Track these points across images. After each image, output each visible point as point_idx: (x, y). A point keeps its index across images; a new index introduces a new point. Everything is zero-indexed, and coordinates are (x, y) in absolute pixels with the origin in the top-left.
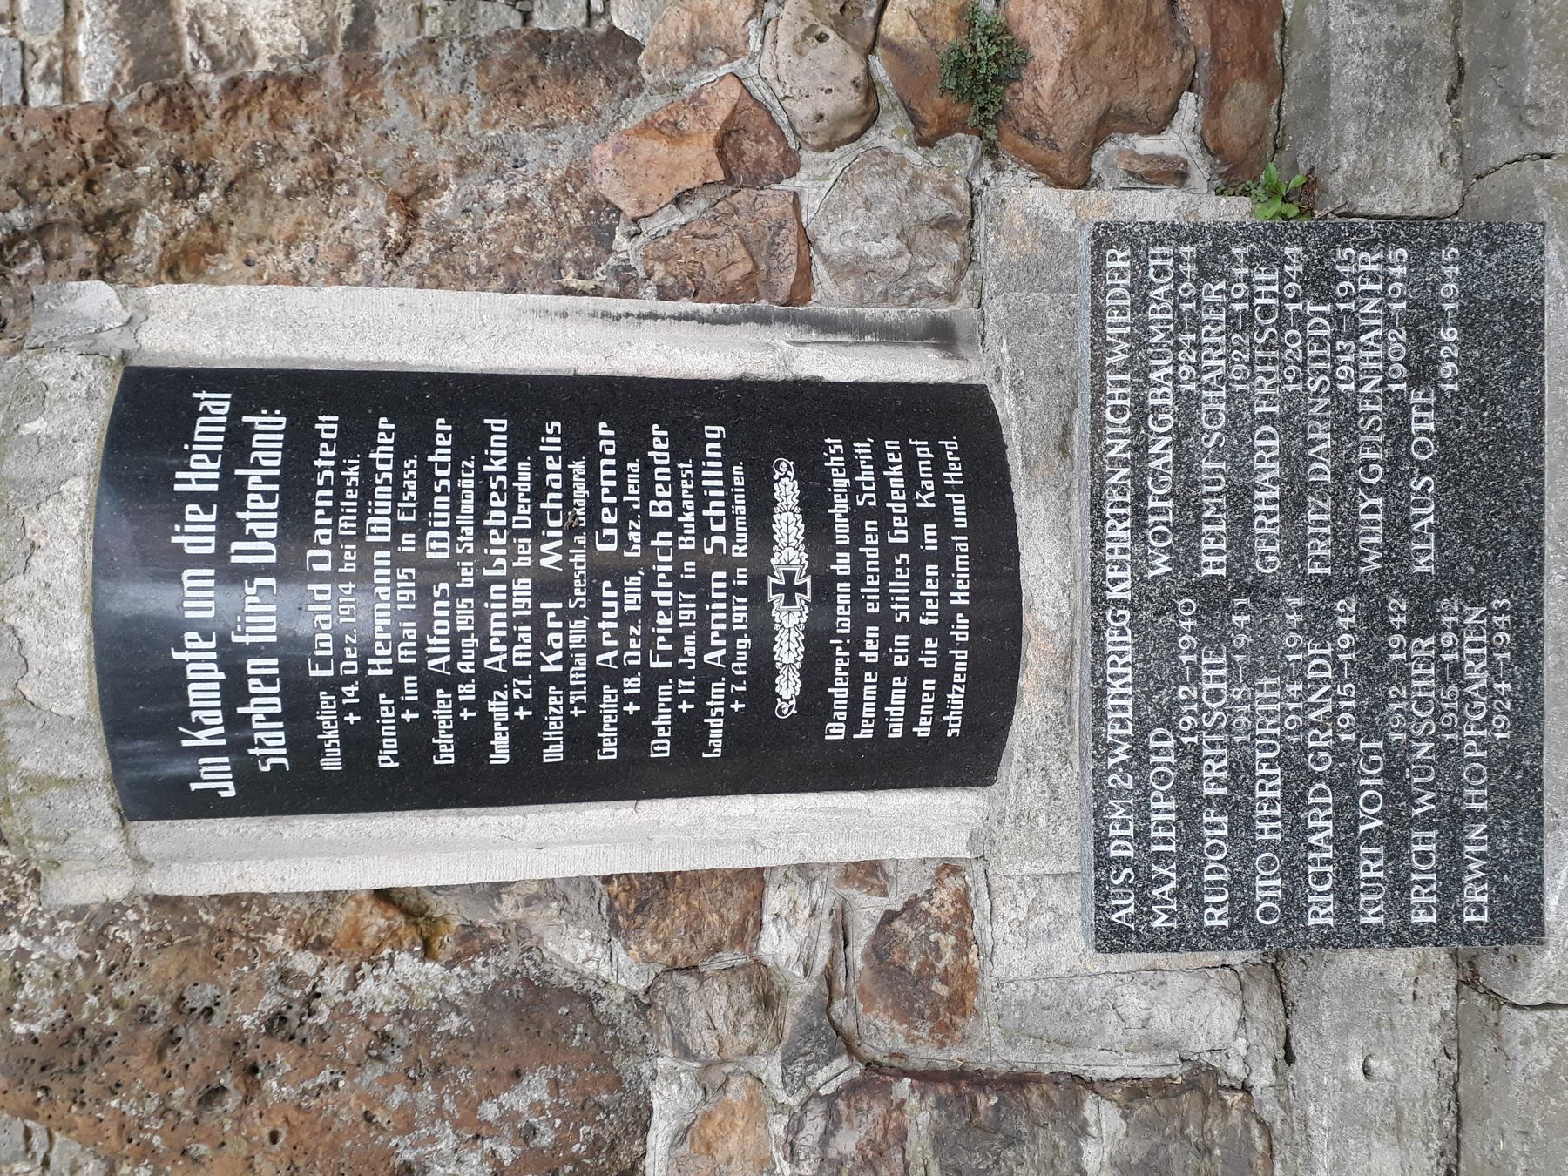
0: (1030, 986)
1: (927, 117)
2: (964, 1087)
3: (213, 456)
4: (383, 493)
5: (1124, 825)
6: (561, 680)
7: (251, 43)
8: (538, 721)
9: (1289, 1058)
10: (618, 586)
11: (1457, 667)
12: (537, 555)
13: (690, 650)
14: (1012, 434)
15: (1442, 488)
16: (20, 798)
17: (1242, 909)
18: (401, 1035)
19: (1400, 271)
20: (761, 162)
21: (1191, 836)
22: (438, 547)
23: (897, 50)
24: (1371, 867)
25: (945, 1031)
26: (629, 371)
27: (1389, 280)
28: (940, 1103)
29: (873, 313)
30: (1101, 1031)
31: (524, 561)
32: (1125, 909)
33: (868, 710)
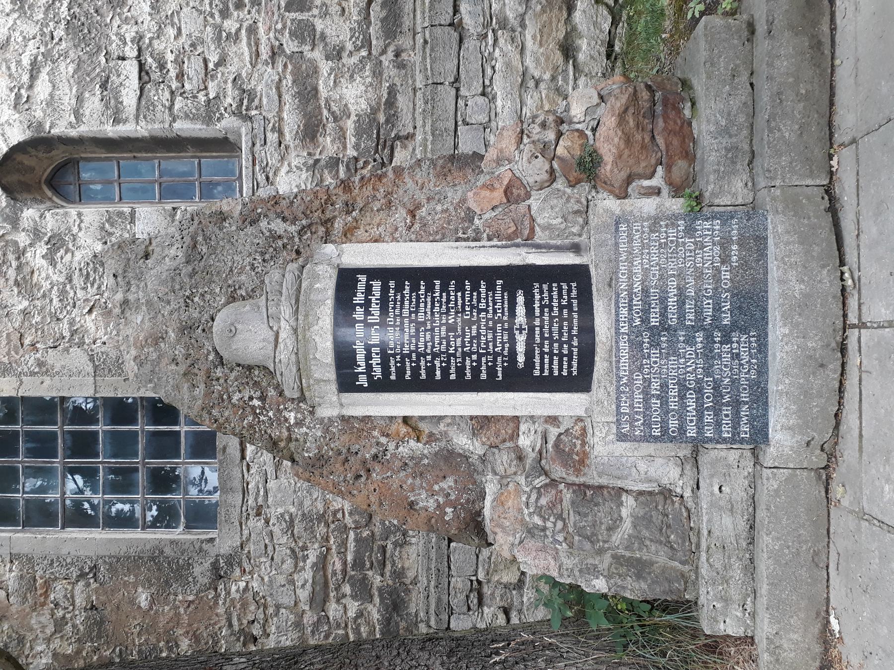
0: (606, 458)
1: (571, 179)
2: (582, 487)
3: (362, 293)
4: (407, 303)
5: (626, 402)
6: (454, 355)
7: (348, 109)
8: (448, 367)
9: (698, 488)
10: (470, 328)
11: (738, 355)
12: (447, 320)
13: (491, 347)
14: (594, 281)
15: (732, 297)
16: (313, 385)
17: (665, 430)
18: (410, 464)
19: (717, 227)
20: (519, 196)
21: (647, 407)
22: (421, 317)
23: (561, 159)
24: (709, 418)
25: (578, 472)
26: (475, 264)
27: (714, 230)
28: (574, 492)
29: (552, 242)
30: (631, 475)
31: (444, 322)
32: (626, 428)
33: (546, 366)
